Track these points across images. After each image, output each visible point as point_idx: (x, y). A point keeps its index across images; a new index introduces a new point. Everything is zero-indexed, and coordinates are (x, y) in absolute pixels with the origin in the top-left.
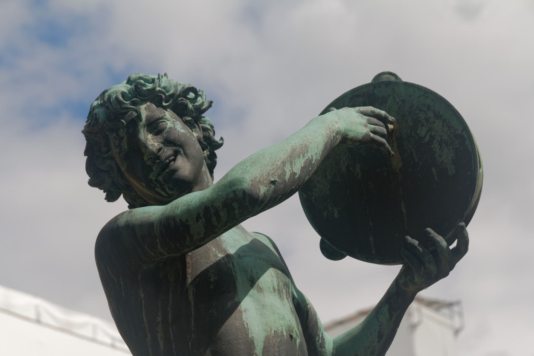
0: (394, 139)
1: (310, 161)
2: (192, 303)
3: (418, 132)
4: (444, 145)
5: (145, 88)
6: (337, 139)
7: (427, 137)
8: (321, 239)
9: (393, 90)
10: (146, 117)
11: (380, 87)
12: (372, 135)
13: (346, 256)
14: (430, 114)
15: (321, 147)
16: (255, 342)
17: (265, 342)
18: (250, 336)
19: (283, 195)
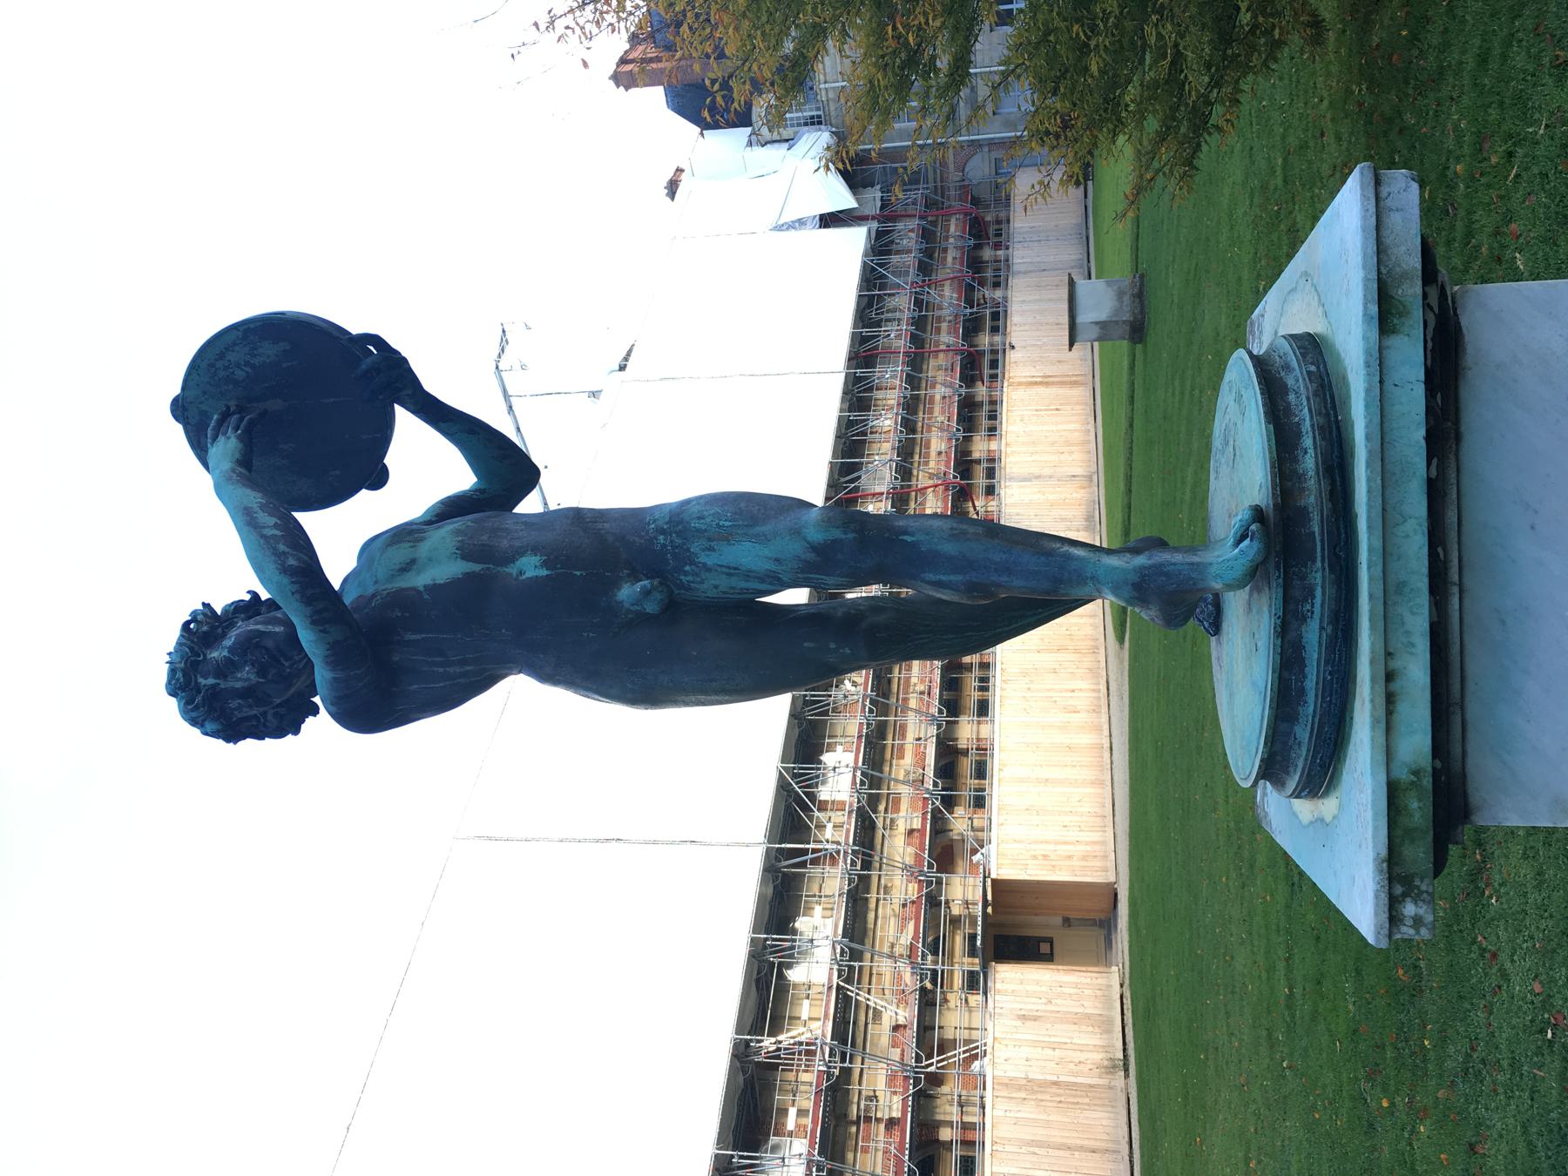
0: (248, 405)
1: (263, 507)
2: (424, 636)
3: (241, 379)
4: (255, 352)
5: (182, 680)
6: (240, 473)
7: (247, 369)
8: (367, 488)
9: (191, 403)
10: (215, 679)
11: (187, 418)
12: (239, 432)
13: (385, 465)
14: (219, 364)
15: (248, 491)
16: (467, 571)
17: (468, 561)
18: (461, 576)
19: (471, 432)
